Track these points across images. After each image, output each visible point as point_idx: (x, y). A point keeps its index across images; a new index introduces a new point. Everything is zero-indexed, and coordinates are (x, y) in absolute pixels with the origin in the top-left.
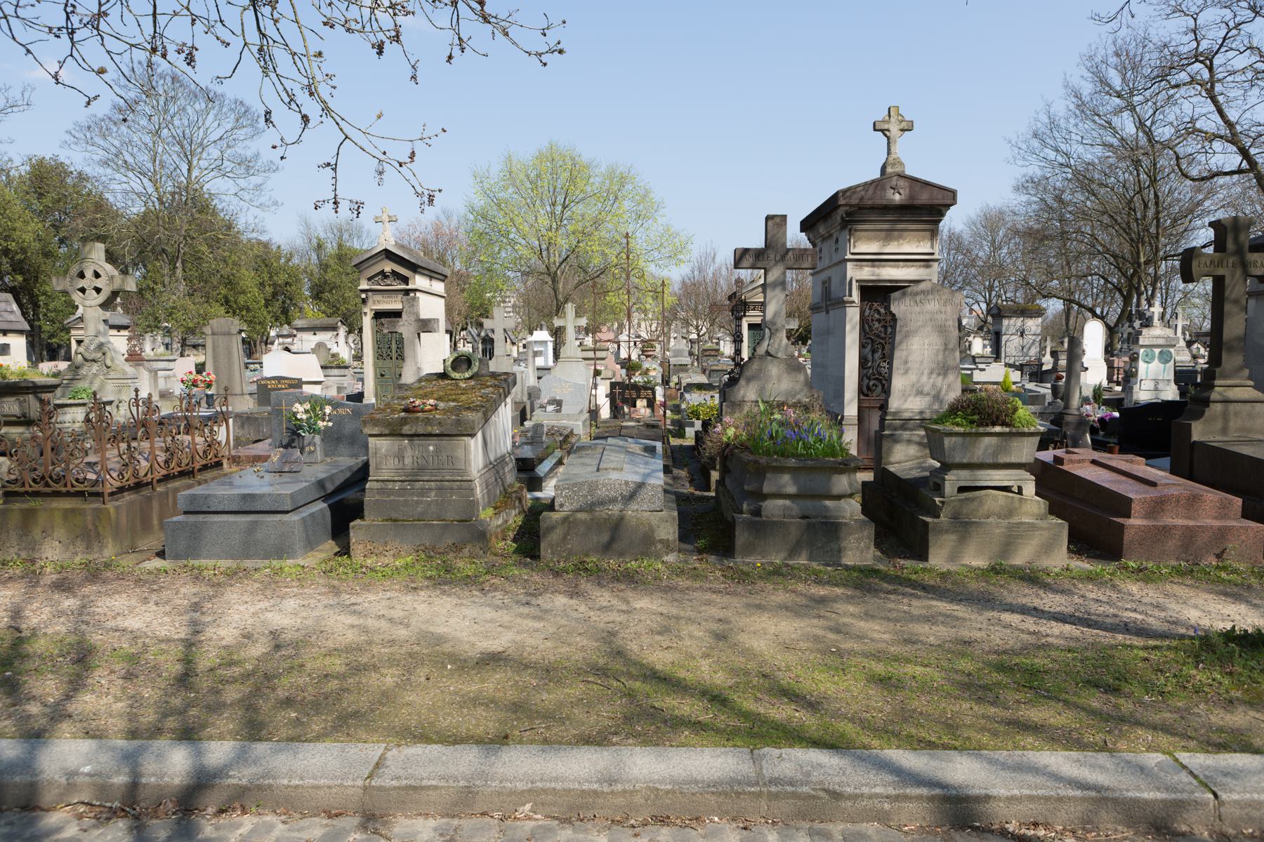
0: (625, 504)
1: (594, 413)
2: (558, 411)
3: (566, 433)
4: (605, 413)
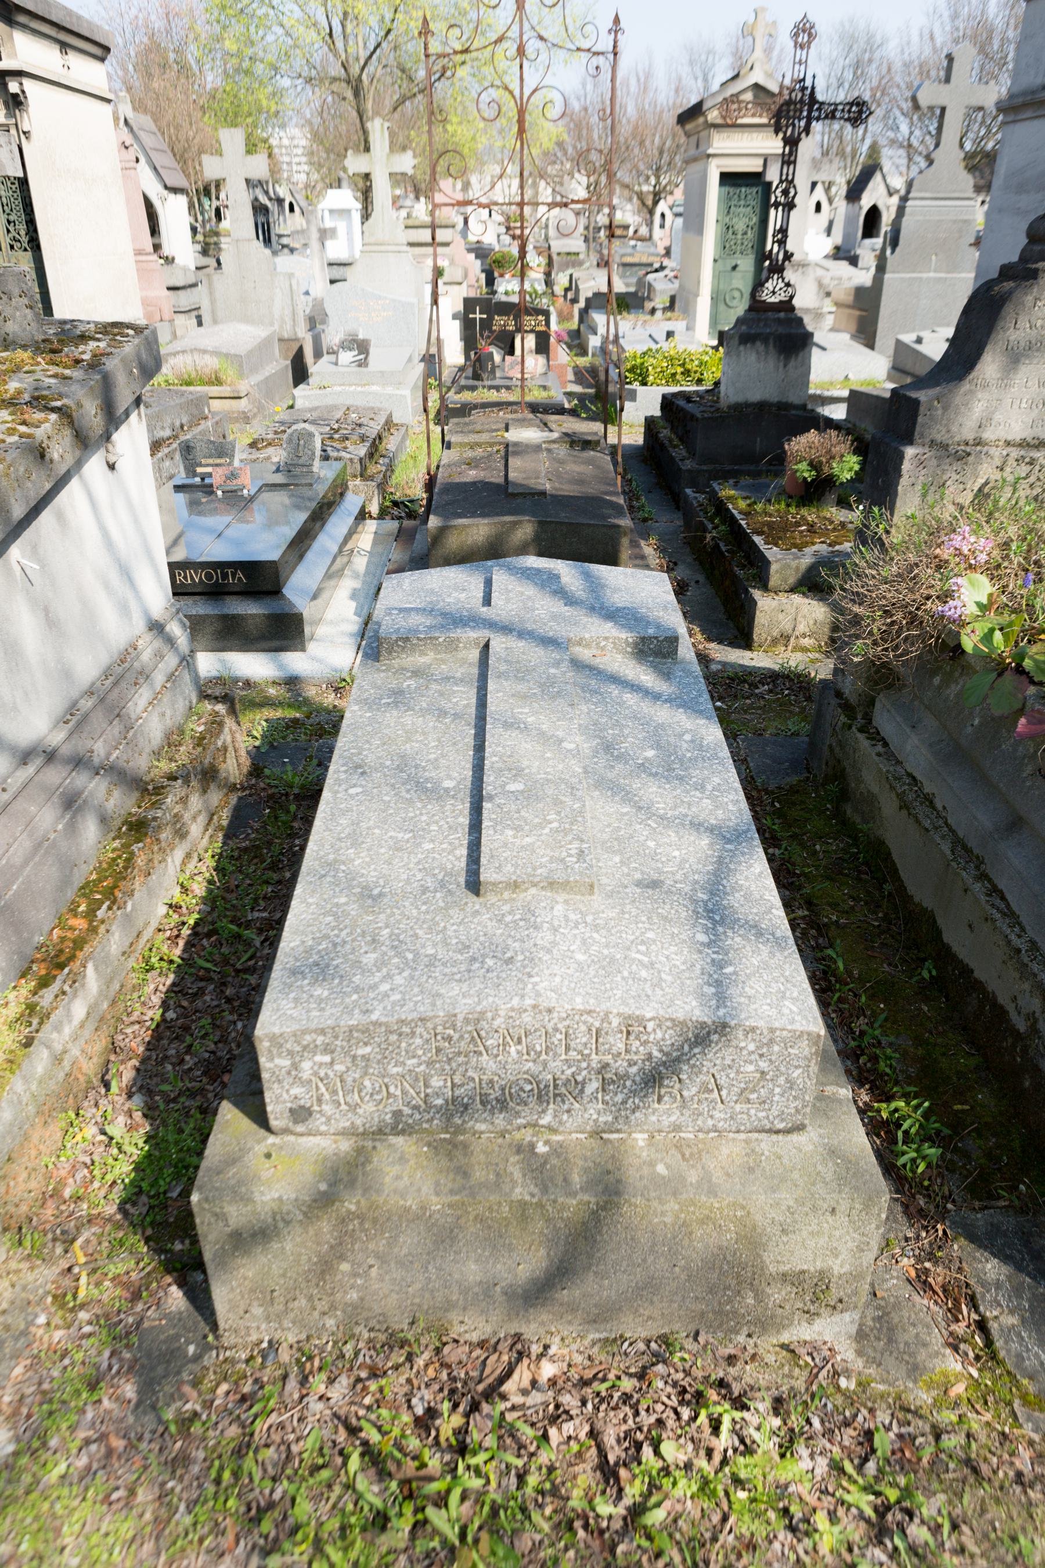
0: (622, 1114)
1: (431, 361)
2: (363, 364)
3: (373, 428)
4: (454, 354)
